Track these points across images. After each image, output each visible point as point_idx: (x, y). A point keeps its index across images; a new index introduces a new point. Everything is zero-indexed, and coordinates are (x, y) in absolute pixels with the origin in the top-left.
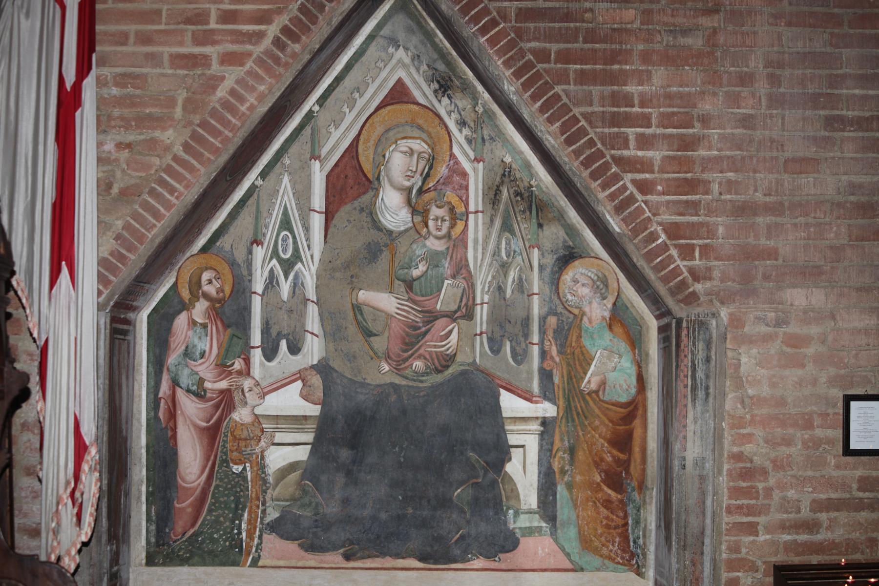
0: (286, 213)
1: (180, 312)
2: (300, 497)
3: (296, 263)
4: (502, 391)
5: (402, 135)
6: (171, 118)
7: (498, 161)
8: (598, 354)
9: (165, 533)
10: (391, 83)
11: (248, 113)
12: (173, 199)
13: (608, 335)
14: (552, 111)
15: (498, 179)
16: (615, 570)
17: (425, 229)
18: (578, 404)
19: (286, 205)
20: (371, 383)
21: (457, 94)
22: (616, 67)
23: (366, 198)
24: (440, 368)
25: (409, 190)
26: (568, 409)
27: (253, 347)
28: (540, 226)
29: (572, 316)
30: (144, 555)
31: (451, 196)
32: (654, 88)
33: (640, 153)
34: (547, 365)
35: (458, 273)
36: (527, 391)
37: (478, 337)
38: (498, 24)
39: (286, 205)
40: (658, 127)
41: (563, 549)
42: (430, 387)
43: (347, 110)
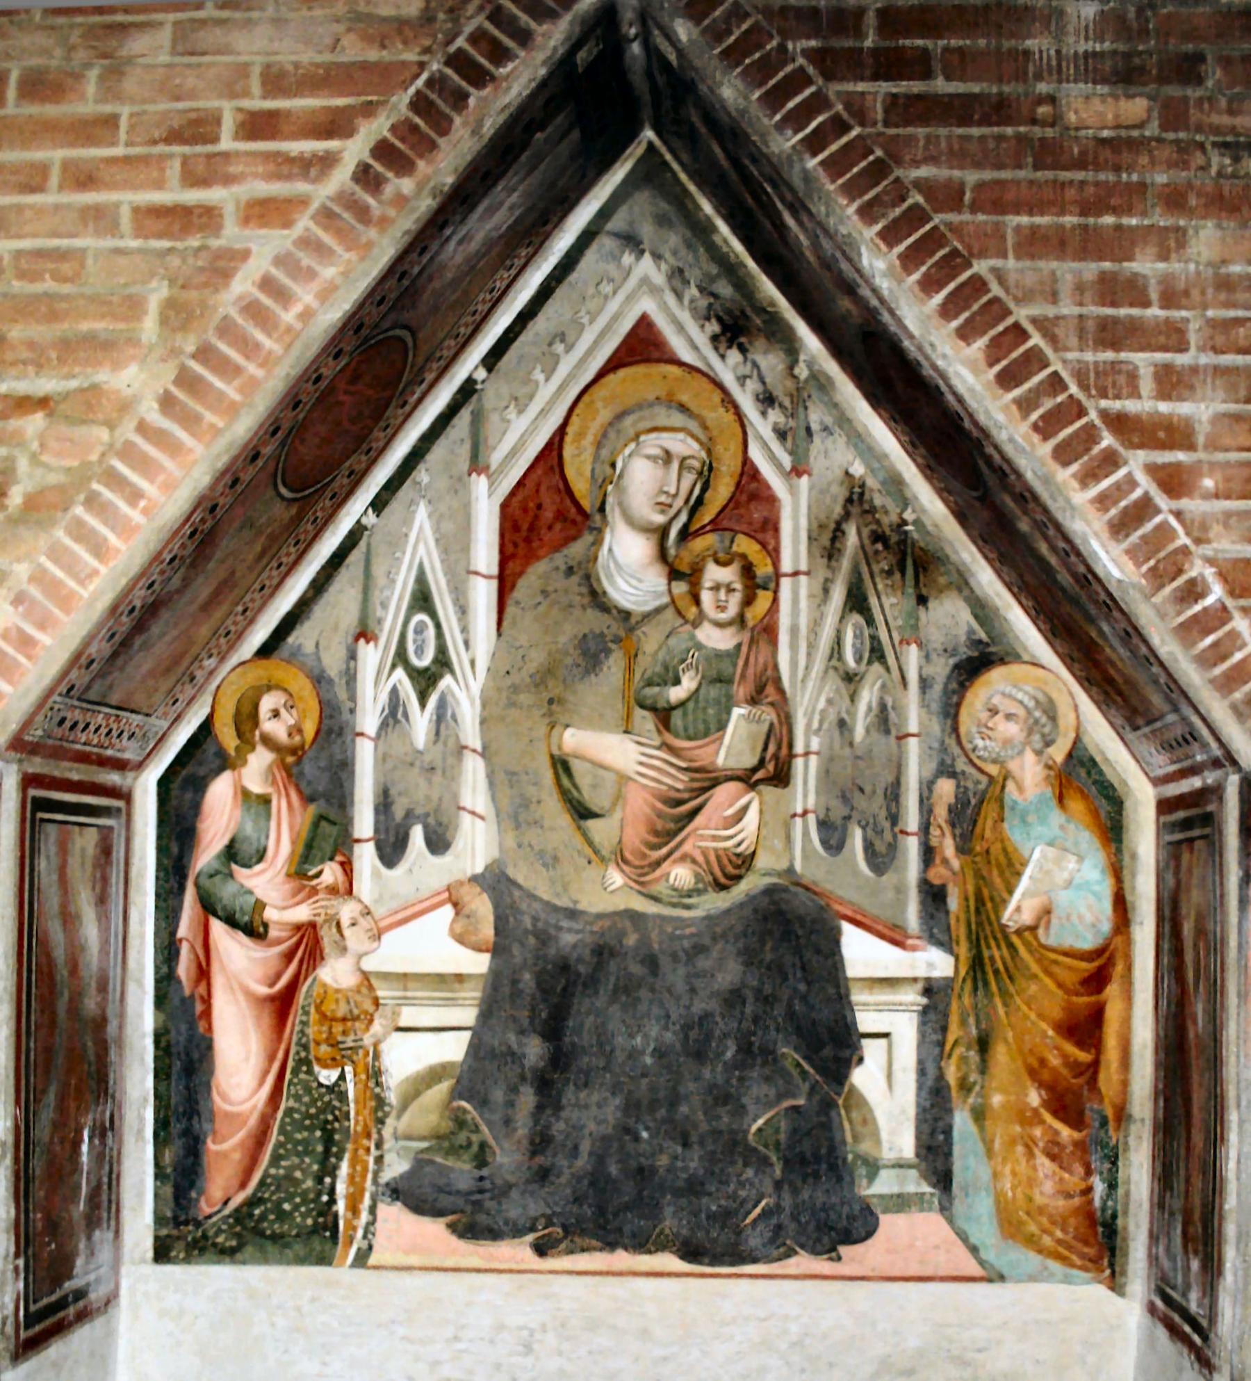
0: (421, 580)
1: (221, 769)
2: (453, 1136)
3: (441, 676)
4: (846, 927)
5: (649, 425)
6: (133, 342)
7: (839, 473)
8: (1037, 855)
9: (190, 1200)
11: (298, 326)
12: (135, 515)
13: (1056, 817)
14: (966, 315)
16: (1067, 1280)
17: (694, 609)
18: (996, 953)
19: (421, 566)
22: (1108, 220)
23: (577, 549)
24: (723, 880)
26: (977, 963)
27: (358, 841)
28: (922, 600)
29: (984, 780)
30: (149, 1243)
32: (1192, 267)
33: (1164, 407)
34: (937, 874)
36: (895, 927)
38: (846, 128)
39: (421, 566)
40: (1202, 349)
41: (963, 1237)
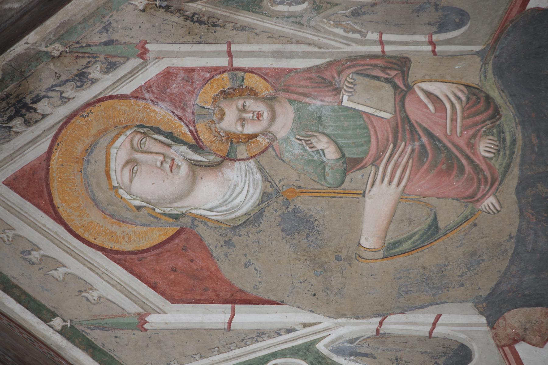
3: (318, 352)
5: (103, 177)
7: (144, 18)
10: (15, 198)
15: (175, 18)
17: (259, 139)
20: (517, 225)
21: (32, 88)
23: (210, 237)
24: (490, 112)
25: (194, 165)
31: (204, 98)
35: (330, 84)
37: (438, 48)
42: (523, 128)
43: (62, 270)
